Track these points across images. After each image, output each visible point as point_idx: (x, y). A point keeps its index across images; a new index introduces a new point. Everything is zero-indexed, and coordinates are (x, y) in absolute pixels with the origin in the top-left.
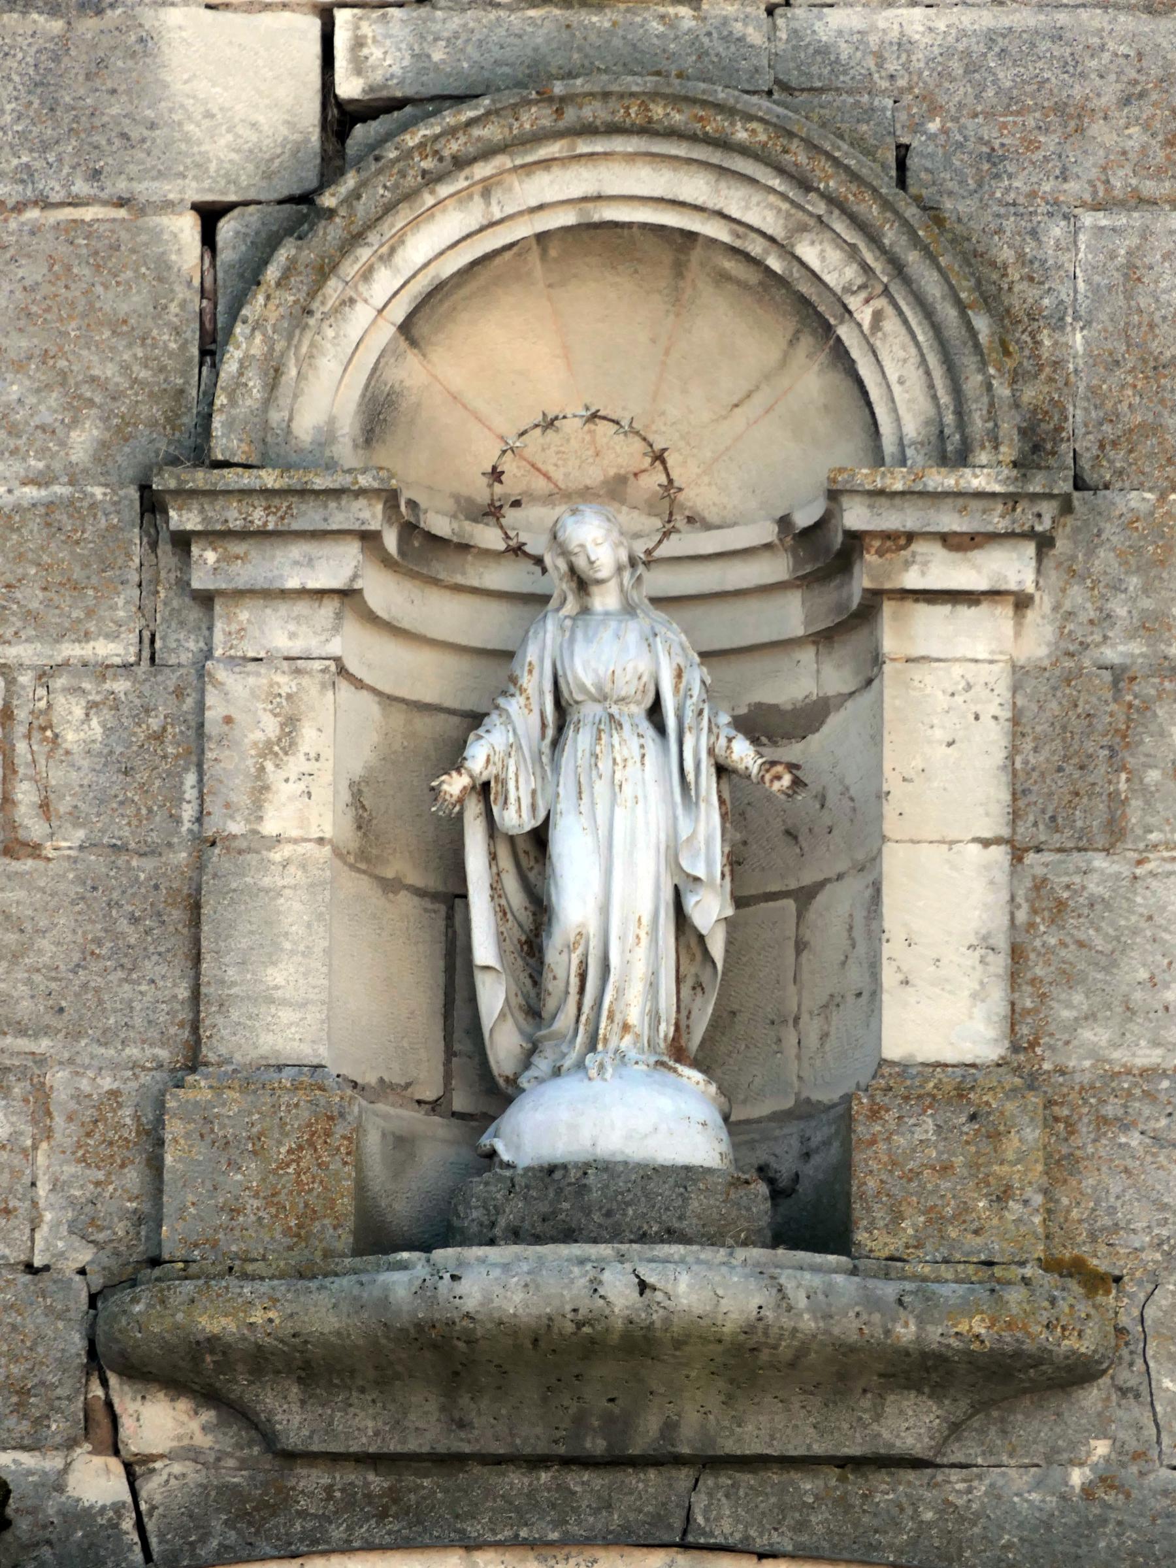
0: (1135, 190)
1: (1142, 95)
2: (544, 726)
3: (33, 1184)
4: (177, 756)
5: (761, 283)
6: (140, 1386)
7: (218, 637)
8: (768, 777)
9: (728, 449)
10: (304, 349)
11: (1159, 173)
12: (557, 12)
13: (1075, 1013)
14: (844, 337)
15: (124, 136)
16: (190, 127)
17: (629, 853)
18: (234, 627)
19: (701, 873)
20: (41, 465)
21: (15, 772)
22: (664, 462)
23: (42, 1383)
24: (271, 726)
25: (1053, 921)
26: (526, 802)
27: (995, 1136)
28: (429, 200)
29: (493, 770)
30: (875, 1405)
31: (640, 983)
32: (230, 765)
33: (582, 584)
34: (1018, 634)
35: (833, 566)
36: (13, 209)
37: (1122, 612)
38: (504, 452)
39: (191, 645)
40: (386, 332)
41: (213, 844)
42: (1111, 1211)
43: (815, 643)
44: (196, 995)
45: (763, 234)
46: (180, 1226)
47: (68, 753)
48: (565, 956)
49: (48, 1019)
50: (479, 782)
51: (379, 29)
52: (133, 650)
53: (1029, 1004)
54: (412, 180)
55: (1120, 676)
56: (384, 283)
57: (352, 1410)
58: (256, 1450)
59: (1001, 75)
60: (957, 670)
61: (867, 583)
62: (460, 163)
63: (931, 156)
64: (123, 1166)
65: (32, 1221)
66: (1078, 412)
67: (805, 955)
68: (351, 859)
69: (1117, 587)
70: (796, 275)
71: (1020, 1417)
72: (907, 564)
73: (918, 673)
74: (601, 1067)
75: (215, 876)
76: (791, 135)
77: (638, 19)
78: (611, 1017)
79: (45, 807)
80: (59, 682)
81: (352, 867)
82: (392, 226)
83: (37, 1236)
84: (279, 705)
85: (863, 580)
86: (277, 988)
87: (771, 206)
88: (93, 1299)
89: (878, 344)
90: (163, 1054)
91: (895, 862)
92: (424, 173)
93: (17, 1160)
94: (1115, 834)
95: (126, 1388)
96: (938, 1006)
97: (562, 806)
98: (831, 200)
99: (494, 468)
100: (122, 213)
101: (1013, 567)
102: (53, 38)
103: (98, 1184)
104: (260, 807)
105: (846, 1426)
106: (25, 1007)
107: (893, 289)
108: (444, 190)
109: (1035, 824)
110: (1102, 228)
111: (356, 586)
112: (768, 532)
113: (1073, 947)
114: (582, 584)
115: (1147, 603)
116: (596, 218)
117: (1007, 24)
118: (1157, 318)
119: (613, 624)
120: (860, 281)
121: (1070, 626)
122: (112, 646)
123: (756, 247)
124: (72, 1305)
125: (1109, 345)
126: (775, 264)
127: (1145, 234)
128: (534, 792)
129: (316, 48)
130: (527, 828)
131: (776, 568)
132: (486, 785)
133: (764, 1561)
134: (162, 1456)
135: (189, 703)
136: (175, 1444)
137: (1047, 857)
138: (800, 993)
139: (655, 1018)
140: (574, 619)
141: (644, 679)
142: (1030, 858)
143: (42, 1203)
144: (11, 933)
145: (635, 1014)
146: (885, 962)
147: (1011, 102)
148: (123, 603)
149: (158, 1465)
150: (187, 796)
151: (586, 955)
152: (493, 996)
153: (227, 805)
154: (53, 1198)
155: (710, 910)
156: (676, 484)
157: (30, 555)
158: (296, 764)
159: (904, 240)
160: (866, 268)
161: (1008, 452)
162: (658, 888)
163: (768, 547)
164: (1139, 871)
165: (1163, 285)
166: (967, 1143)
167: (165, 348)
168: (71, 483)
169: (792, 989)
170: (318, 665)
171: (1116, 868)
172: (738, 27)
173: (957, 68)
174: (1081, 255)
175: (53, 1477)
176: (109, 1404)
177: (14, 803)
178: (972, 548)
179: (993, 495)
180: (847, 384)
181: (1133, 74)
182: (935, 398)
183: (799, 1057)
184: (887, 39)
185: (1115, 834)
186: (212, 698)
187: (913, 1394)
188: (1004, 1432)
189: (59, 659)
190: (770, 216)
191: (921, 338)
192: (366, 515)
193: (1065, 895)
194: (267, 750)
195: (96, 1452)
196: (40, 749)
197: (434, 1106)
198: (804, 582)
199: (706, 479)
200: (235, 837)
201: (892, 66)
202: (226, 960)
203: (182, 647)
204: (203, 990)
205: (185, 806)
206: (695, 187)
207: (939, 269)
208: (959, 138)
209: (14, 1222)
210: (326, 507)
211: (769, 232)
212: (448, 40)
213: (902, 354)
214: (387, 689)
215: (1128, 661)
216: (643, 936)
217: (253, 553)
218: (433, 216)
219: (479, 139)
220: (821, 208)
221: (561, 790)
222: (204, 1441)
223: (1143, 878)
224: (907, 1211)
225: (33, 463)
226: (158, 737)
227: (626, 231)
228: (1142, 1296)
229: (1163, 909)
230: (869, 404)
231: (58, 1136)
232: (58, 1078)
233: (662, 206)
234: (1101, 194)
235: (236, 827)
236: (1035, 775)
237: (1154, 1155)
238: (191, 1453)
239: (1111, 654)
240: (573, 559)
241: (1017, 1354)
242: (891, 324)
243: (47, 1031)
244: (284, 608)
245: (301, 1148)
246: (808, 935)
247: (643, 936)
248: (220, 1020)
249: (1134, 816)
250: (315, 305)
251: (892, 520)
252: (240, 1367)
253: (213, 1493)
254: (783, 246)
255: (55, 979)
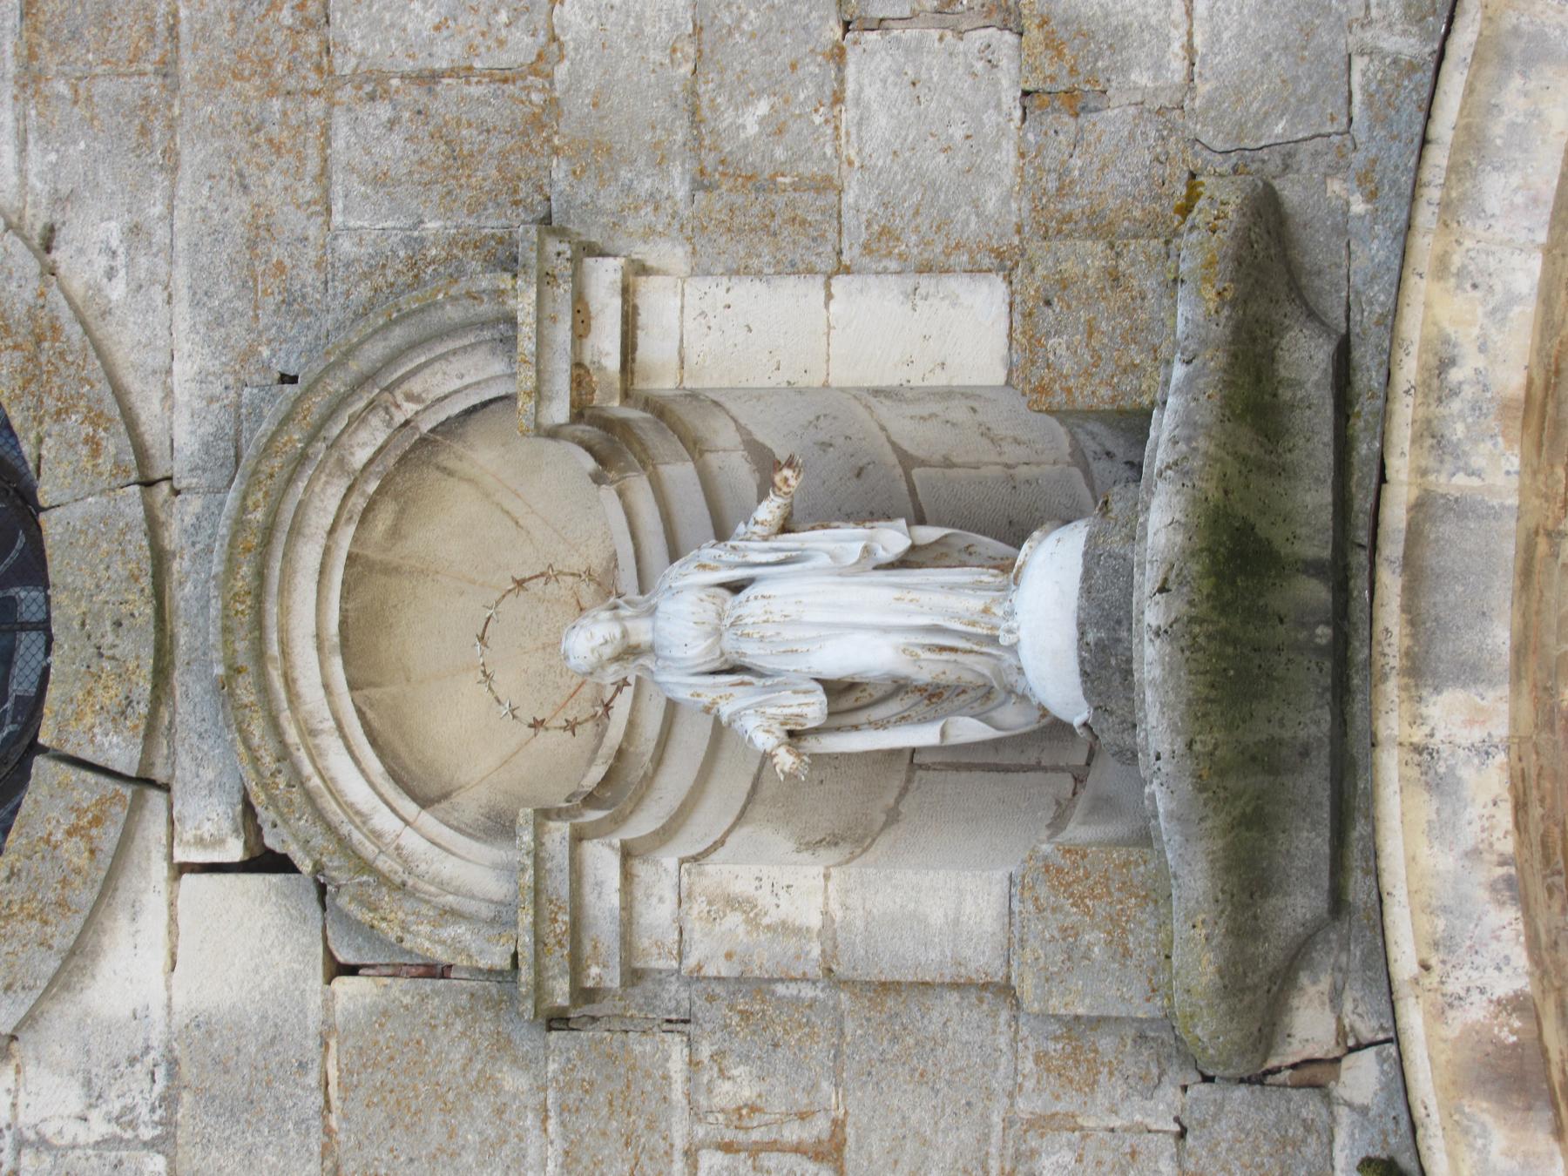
0: (314, 179)
1: (241, 175)
2: (742, 683)
3: (1112, 1130)
4: (763, 1002)
5: (395, 499)
6: (1279, 1039)
7: (661, 964)
8: (785, 489)
9: (555, 531)
10: (433, 889)
11: (301, 159)
12: (176, 674)
13: (973, 218)
14: (430, 427)
15: (272, 1042)
16: (266, 986)
17: (841, 609)
18: (654, 950)
19: (861, 545)
20: (530, 1116)
21: (775, 1141)
22: (524, 581)
23: (1276, 1125)
24: (734, 919)
25: (898, 239)
26: (802, 699)
27: (1064, 284)
28: (315, 781)
29: (776, 727)
30: (1290, 386)
31: (948, 597)
32: (765, 956)
33: (630, 652)
34: (666, 273)
35: (619, 431)
36: (330, 1137)
37: (648, 183)
38: (514, 717)
39: (673, 988)
40: (426, 819)
41: (830, 970)
42: (1136, 182)
43: (702, 453)
44: (955, 986)
45: (345, 497)
46: (1136, 1001)
47: (760, 1096)
48: (923, 664)
49: (976, 1116)
50: (786, 739)
51: (189, 824)
52: (678, 1038)
53: (965, 258)
54: (296, 795)
55: (701, 183)
56: (384, 821)
57: (1293, 851)
58: (1333, 936)
59: (225, 295)
60: (689, 324)
61: (616, 403)
62: (284, 754)
63: (288, 354)
64: (1096, 1051)
65: (1141, 1132)
66: (489, 224)
67: (955, 460)
68: (858, 851)
69: (628, 189)
70: (381, 468)
71: (1307, 259)
72: (601, 368)
73: (692, 358)
74: (1010, 631)
75: (854, 969)
76: (255, 472)
77: (182, 604)
78: (973, 624)
79: (802, 1116)
80: (703, 1101)
81: (865, 850)
82: (334, 813)
83: (1154, 1127)
84: (717, 912)
85: (614, 406)
86: (946, 915)
87: (323, 490)
88: (1207, 1079)
89: (431, 397)
90: (1004, 1015)
91: (842, 376)
92: (290, 786)
93: (1091, 1143)
94: (826, 185)
95: (1281, 1050)
96: (957, 336)
97: (803, 667)
98: (312, 438)
99: (530, 726)
100: (333, 1043)
101: (604, 276)
102: (198, 1102)
103: (1111, 1073)
104: (800, 929)
105: (1308, 412)
106: (967, 1135)
107: (384, 384)
108: (307, 768)
109: (819, 255)
110: (345, 207)
111: (618, 845)
112: (608, 493)
113: (919, 220)
114: (630, 652)
115: (641, 162)
116: (336, 640)
117: (185, 290)
118: (416, 158)
119: (660, 623)
120: (382, 413)
121: (660, 228)
122: (674, 1057)
123: (358, 502)
124: (1212, 1097)
125: (436, 199)
126: (372, 487)
127: (350, 169)
128: (795, 692)
129: (205, 877)
130: (824, 698)
131: (639, 487)
132: (791, 734)
133: (1388, 477)
134: (1339, 1019)
135: (719, 989)
136: (1327, 1008)
137: (845, 245)
138: (986, 464)
139: (978, 586)
140: (658, 658)
141: (703, 596)
142: (846, 259)
143: (1126, 1123)
144: (921, 1148)
145: (972, 603)
146: (926, 383)
147: (248, 285)
148: (641, 1046)
149: (1346, 1022)
150: (795, 993)
151: (923, 646)
152: (968, 729)
153: (798, 957)
154: (1123, 1114)
155: (893, 538)
156: (544, 569)
157: (602, 1126)
158: (764, 898)
159: (341, 374)
160: (371, 406)
161: (505, 281)
162: (871, 584)
163: (621, 494)
164: (857, 164)
165: (389, 153)
166: (1069, 307)
167: (437, 1008)
168: (545, 1090)
169: (984, 471)
170: (685, 879)
171: (854, 183)
172: (189, 520)
173: (218, 334)
174: (366, 224)
175: (1356, 1116)
176: (1294, 1066)
177: (799, 1144)
178: (588, 312)
179: (539, 294)
180: (474, 426)
181: (224, 182)
182: (473, 346)
183: (1038, 464)
184: (197, 393)
185: (826, 185)
186: (710, 971)
187: (1278, 352)
188: (1319, 273)
189: (685, 1102)
190: (331, 490)
191: (423, 359)
192: (557, 836)
193: (876, 227)
194: (753, 923)
195: (1337, 1078)
196: (757, 1119)
197: (1079, 780)
198: (647, 463)
199: (583, 548)
200: (823, 951)
201: (218, 389)
202: (923, 959)
203: (674, 995)
204: (947, 980)
205: (803, 994)
206: (309, 555)
207: (361, 343)
208: (274, 330)
209: (1142, 1148)
210: (550, 871)
211: (344, 491)
212: (198, 766)
213: (439, 376)
214: (730, 820)
215: (688, 177)
216: (910, 596)
217: (592, 933)
218: (331, 779)
219: (262, 737)
220: (321, 446)
221: (792, 668)
222: (1325, 983)
223: (863, 160)
224: (1125, 361)
225: (528, 1123)
226: (745, 1015)
227: (351, 614)
228: (1206, 153)
229: (887, 142)
230: (485, 404)
231: (1072, 1109)
232: (1025, 1107)
233: (325, 582)
234: (318, 208)
235: (816, 951)
236: (779, 256)
237: (1089, 145)
238: (1336, 996)
239: (681, 191)
240: (605, 657)
241: (1239, 261)
242: (415, 386)
243: (985, 1117)
244: (639, 908)
245: (1072, 895)
246: (937, 457)
247: (910, 596)
248: (972, 966)
249: (809, 169)
250: (398, 880)
251: (561, 384)
252: (1251, 950)
253: (1369, 974)
254: (356, 479)
255: (943, 1110)
